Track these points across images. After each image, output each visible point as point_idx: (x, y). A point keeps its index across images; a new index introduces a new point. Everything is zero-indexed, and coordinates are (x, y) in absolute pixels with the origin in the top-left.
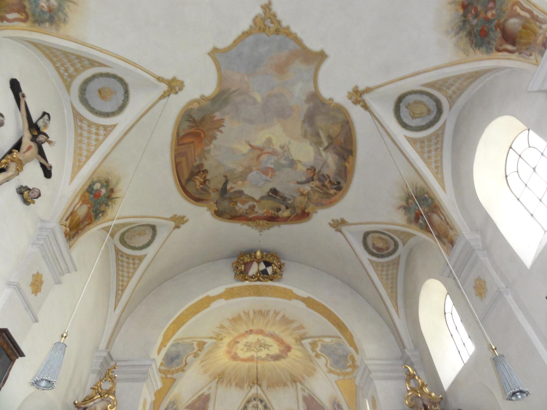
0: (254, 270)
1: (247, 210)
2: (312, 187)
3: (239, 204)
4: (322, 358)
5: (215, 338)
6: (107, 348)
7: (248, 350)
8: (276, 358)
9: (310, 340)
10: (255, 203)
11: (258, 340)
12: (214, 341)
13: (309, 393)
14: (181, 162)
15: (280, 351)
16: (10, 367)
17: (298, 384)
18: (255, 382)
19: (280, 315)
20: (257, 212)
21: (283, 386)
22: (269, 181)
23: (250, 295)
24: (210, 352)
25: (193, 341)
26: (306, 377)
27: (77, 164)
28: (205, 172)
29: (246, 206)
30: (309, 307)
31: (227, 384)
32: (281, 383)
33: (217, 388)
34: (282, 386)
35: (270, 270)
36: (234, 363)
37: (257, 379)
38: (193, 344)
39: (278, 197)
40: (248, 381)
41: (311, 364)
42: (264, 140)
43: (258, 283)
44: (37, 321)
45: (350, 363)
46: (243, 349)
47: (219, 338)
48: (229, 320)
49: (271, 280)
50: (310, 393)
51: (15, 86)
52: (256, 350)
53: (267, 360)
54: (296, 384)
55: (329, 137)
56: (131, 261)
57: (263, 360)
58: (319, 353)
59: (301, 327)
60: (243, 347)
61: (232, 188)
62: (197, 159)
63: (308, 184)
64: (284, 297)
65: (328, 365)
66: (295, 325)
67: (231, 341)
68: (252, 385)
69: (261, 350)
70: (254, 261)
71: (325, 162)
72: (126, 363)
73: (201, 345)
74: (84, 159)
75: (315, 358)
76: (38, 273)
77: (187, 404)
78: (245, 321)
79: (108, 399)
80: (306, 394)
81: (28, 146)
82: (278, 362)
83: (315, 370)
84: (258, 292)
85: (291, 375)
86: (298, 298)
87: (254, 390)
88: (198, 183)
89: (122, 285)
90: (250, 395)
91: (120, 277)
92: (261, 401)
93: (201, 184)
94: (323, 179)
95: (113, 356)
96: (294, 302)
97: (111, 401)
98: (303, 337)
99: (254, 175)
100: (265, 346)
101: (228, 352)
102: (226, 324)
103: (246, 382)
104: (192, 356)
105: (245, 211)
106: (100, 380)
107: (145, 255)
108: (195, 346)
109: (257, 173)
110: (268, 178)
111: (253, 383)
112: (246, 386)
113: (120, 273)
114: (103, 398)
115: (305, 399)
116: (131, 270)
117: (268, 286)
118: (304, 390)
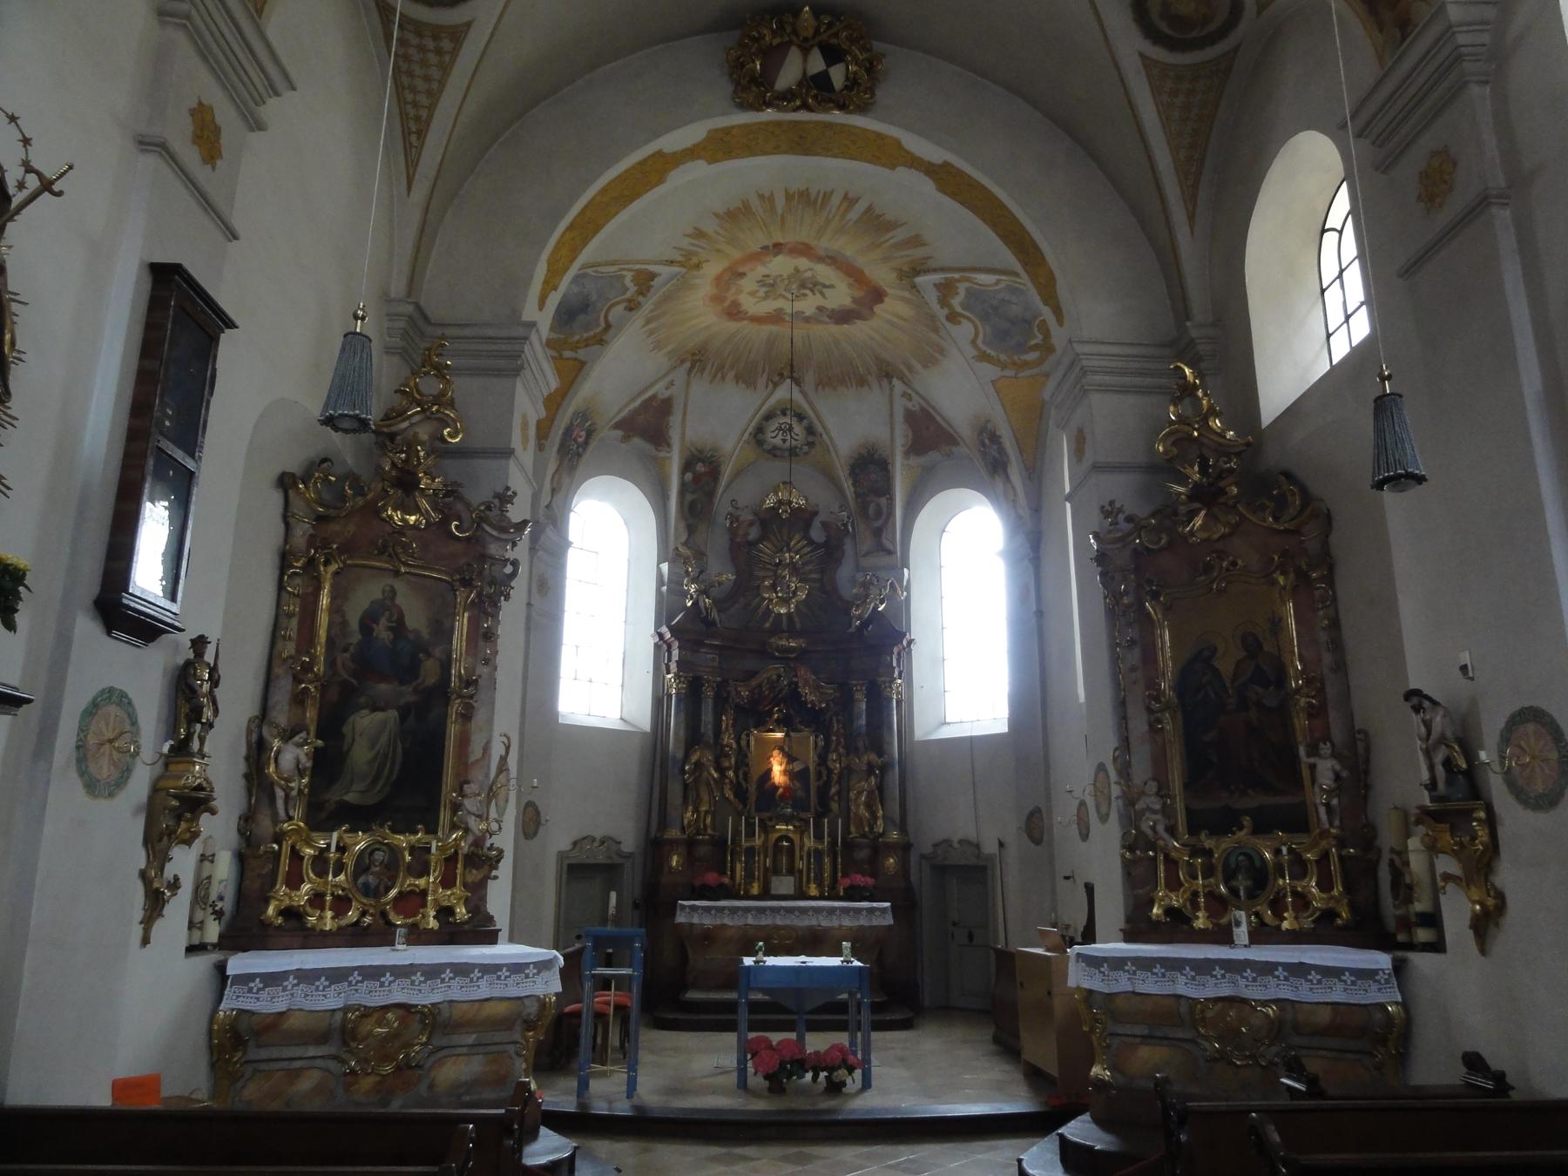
0: (789, 75)
4: (964, 322)
5: (681, 264)
6: (409, 294)
7: (767, 296)
9: (937, 277)
11: (797, 270)
12: (675, 269)
13: (919, 404)
15: (854, 300)
16: (212, 354)
17: (895, 382)
19: (861, 207)
23: (777, 150)
24: (667, 298)
25: (624, 269)
26: (918, 367)
30: (945, 193)
31: (715, 377)
33: (688, 384)
35: (837, 75)
36: (732, 326)
37: (792, 366)
38: (623, 277)
40: (766, 371)
41: (934, 336)
43: (803, 116)
44: (235, 237)
46: (757, 291)
47: (689, 263)
48: (716, 215)
49: (842, 107)
50: (924, 404)
52: (790, 296)
53: (819, 322)
54: (890, 383)
57: (807, 320)
58: (959, 309)
59: (916, 241)
60: (755, 286)
64: (875, 160)
65: (979, 342)
66: (900, 235)
67: (725, 271)
68: (776, 379)
69: (805, 295)
70: (790, 43)
72: (467, 332)
73: (645, 280)
76: (200, 104)
78: (762, 219)
79: (439, 415)
80: (914, 406)
83: (942, 351)
84: (801, 142)
86: (915, 163)
87: (783, 392)
89: (417, 119)
90: (772, 401)
92: (801, 417)
95: (429, 313)
96: (904, 174)
97: (450, 421)
98: (917, 269)
100: (814, 286)
101: (717, 299)
102: (710, 227)
103: (763, 372)
104: (620, 308)
106: (413, 374)
107: (469, 25)
108: (628, 281)
111: (781, 375)
112: (762, 381)
114: (428, 413)
115: (910, 417)
116: (435, 73)
117: (829, 126)
118: (910, 395)
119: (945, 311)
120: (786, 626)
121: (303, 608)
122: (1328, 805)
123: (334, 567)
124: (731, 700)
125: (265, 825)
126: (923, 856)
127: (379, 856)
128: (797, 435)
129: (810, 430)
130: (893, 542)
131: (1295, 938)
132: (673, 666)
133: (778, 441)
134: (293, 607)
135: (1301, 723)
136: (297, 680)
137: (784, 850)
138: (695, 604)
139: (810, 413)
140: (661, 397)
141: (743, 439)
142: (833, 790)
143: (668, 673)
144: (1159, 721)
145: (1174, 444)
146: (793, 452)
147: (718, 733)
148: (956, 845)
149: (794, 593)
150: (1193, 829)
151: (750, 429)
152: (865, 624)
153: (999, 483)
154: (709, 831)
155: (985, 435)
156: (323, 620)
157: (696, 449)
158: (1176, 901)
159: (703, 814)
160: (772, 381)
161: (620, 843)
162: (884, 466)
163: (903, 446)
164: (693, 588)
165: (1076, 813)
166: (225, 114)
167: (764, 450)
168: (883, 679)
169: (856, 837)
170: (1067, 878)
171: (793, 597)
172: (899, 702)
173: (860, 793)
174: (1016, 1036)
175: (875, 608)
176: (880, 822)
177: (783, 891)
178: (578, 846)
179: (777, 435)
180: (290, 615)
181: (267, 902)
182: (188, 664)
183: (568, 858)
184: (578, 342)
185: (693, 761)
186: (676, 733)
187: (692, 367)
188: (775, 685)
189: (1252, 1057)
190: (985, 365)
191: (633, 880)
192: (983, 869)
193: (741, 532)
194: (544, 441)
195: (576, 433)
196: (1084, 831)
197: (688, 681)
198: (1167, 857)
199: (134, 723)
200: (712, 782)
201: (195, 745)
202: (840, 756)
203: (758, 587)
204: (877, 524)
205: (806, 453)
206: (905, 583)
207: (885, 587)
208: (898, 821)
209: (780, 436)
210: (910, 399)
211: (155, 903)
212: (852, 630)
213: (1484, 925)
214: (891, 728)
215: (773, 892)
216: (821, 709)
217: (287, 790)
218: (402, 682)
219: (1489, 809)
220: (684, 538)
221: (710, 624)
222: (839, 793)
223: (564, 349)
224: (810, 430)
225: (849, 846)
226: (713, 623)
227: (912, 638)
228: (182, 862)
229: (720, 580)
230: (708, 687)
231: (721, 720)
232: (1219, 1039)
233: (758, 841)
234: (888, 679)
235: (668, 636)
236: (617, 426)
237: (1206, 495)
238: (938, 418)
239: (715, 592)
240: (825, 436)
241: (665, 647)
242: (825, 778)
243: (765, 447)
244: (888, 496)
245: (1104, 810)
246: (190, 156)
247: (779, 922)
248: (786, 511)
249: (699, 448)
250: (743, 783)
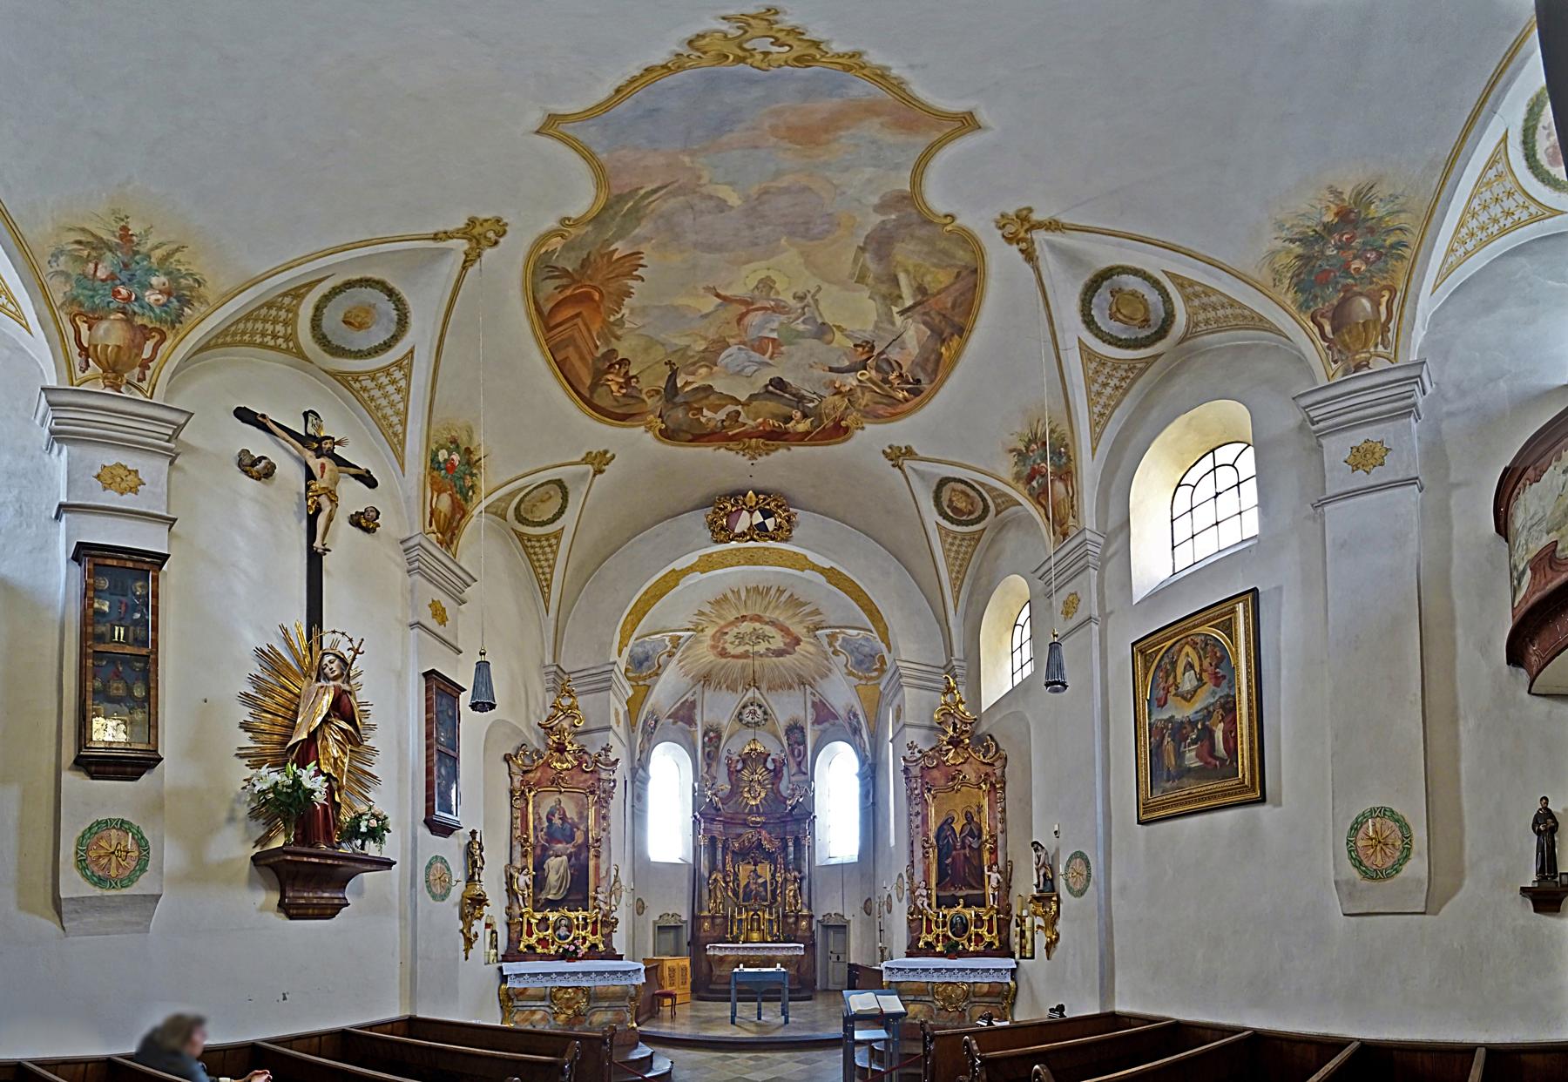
0: (743, 523)
1: (723, 421)
2: (860, 381)
3: (705, 412)
7: (740, 644)
8: (780, 653)
9: (828, 631)
10: (739, 408)
11: (755, 629)
14: (567, 358)
19: (787, 594)
20: (744, 424)
22: (768, 364)
27: (395, 440)
28: (624, 362)
29: (722, 415)
33: (703, 693)
36: (724, 660)
39: (787, 395)
42: (752, 283)
43: (751, 544)
45: (878, 666)
47: (698, 629)
49: (773, 539)
51: (243, 415)
53: (767, 656)
55: (921, 290)
56: (545, 543)
57: (761, 656)
58: (838, 648)
60: (733, 639)
61: (687, 383)
62: (598, 343)
63: (853, 374)
66: (808, 609)
70: (743, 509)
71: (898, 338)
74: (399, 429)
81: (319, 466)
83: (830, 670)
84: (751, 559)
85: (799, 676)
88: (614, 388)
89: (546, 580)
90: (745, 699)
93: (621, 387)
94: (885, 366)
96: (808, 574)
99: (732, 355)
100: (766, 638)
102: (707, 609)
105: (719, 424)
108: (667, 642)
109: (739, 349)
110: (766, 358)
113: (537, 564)
115: (814, 704)
117: (767, 549)
119: (832, 649)
120: (755, 811)
121: (522, 814)
122: (993, 895)
123: (533, 793)
125: (517, 911)
126: (818, 921)
127: (563, 922)
129: (765, 713)
131: (977, 954)
132: (702, 832)
133: (749, 719)
134: (518, 814)
135: (986, 856)
136: (523, 846)
138: (711, 800)
139: (765, 703)
144: (927, 853)
145: (943, 715)
146: (757, 724)
147: (724, 865)
150: (939, 906)
152: (793, 808)
156: (531, 818)
158: (930, 938)
162: (802, 730)
166: (445, 601)
180: (517, 818)
181: (520, 942)
182: (470, 843)
189: (956, 1007)
190: (851, 678)
191: (686, 935)
198: (927, 919)
199: (449, 869)
201: (477, 878)
204: (799, 759)
210: (814, 695)
211: (469, 942)
213: (1050, 946)
217: (523, 895)
218: (567, 843)
219: (1058, 896)
222: (781, 892)
224: (765, 713)
225: (785, 916)
226: (719, 809)
228: (478, 926)
232: (943, 1000)
237: (955, 742)
245: (900, 896)
246: (432, 624)
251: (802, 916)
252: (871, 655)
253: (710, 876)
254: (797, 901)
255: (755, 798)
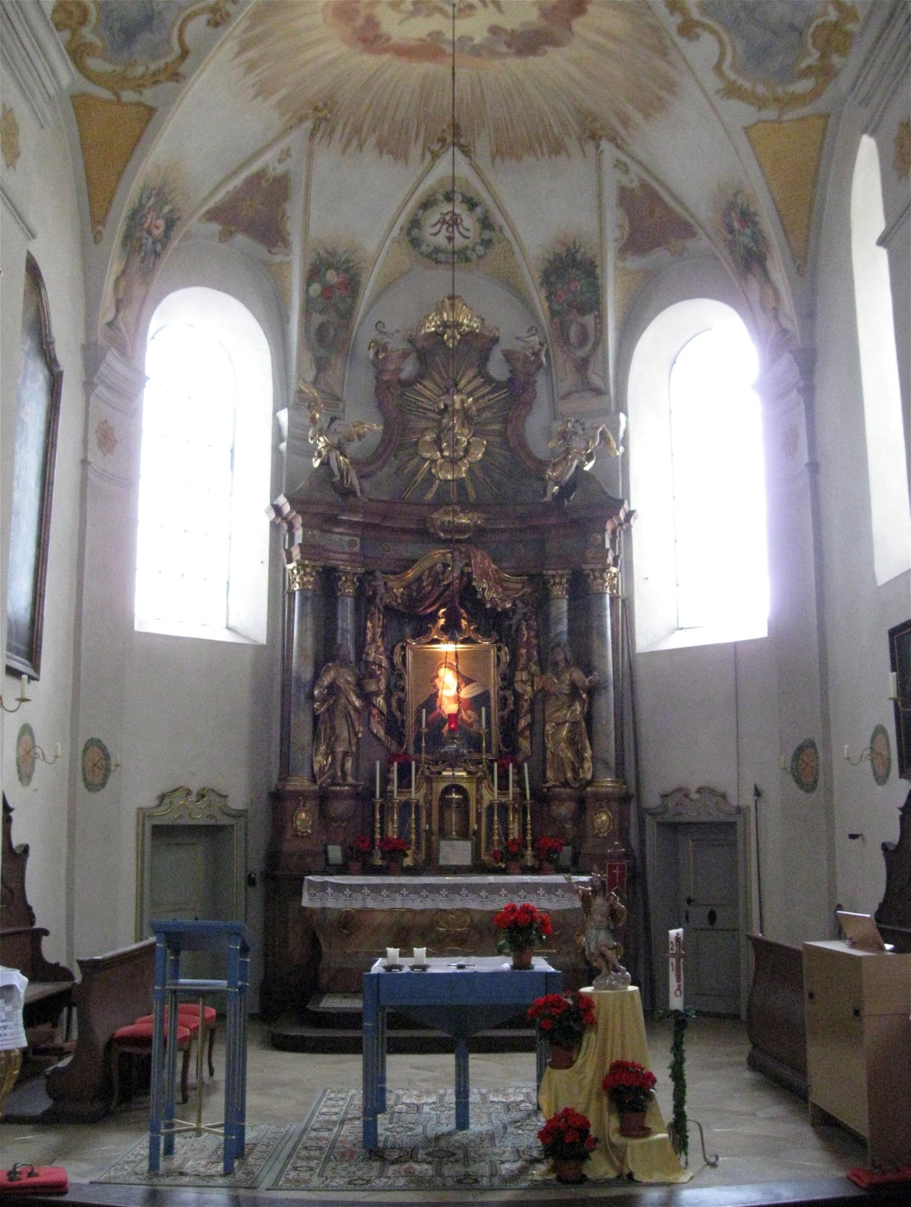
4: (706, 37)
13: (640, 179)
17: (605, 145)
18: (449, 139)
21: (550, 153)
26: (637, 117)
31: (348, 145)
32: (544, 144)
33: (310, 156)
34: (547, 154)
36: (369, 61)
41: (660, 64)
50: (645, 176)
52: (449, 10)
53: (494, 54)
54: (597, 147)
57: (477, 51)
58: (696, 14)
65: (726, 67)
68: (436, 147)
75: (677, 38)
77: (211, 204)
80: (632, 182)
82: (533, 62)
83: (671, 86)
90: (430, 181)
91: (535, 627)
92: (472, 204)
103: (417, 136)
104: (203, 19)
111: (442, 140)
112: (416, 151)
115: (626, 197)
118: (625, 165)
119: (677, 19)
124: (378, 600)
128: (468, 230)
129: (486, 223)
130: (605, 377)
132: (296, 552)
133: (441, 240)
137: (454, 805)
138: (325, 464)
139: (484, 194)
140: (271, 173)
141: (391, 237)
142: (523, 723)
143: (290, 561)
146: (461, 257)
148: (695, 796)
149: (466, 451)
151: (401, 222)
152: (567, 489)
153: (754, 285)
154: (350, 780)
155: (733, 214)
157: (326, 251)
159: (339, 757)
160: (429, 149)
161: (226, 797)
163: (616, 240)
164: (321, 444)
165: (869, 746)
167: (422, 253)
168: (590, 566)
169: (555, 786)
170: (853, 837)
171: (464, 457)
172: (613, 599)
173: (560, 725)
174: (802, 1070)
175: (579, 468)
176: (588, 765)
177: (454, 861)
178: (167, 800)
179: (439, 231)
183: (151, 816)
184: (143, 77)
185: (326, 683)
186: (300, 645)
187: (315, 130)
188: (441, 577)
192: (730, 826)
193: (391, 367)
194: (99, 228)
195: (149, 220)
196: (881, 771)
197: (318, 573)
200: (352, 712)
202: (533, 676)
203: (416, 443)
204: (581, 353)
205: (479, 257)
206: (621, 434)
207: (594, 438)
208: (613, 764)
209: (444, 232)
210: (626, 171)
212: (548, 498)
214: (602, 635)
215: (442, 862)
216: (505, 612)
220: (310, 376)
221: (348, 493)
222: (530, 726)
223: (123, 89)
224: (486, 223)
225: (542, 798)
227: (632, 509)
229: (361, 432)
230: (346, 581)
231: (365, 627)
233: (416, 794)
234: (600, 566)
235: (287, 508)
236: (213, 215)
238: (666, 197)
239: (353, 448)
240: (507, 232)
241: (285, 526)
242: (512, 707)
243: (424, 248)
244: (596, 313)
247: (444, 905)
248: (454, 337)
249: (330, 249)
250: (398, 714)
251: (597, 797)
252: (792, 27)
253: (316, 677)
254: (579, 754)
255: (453, 462)
